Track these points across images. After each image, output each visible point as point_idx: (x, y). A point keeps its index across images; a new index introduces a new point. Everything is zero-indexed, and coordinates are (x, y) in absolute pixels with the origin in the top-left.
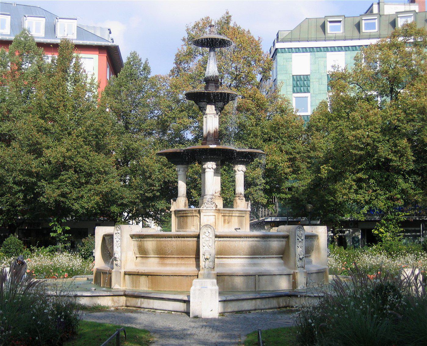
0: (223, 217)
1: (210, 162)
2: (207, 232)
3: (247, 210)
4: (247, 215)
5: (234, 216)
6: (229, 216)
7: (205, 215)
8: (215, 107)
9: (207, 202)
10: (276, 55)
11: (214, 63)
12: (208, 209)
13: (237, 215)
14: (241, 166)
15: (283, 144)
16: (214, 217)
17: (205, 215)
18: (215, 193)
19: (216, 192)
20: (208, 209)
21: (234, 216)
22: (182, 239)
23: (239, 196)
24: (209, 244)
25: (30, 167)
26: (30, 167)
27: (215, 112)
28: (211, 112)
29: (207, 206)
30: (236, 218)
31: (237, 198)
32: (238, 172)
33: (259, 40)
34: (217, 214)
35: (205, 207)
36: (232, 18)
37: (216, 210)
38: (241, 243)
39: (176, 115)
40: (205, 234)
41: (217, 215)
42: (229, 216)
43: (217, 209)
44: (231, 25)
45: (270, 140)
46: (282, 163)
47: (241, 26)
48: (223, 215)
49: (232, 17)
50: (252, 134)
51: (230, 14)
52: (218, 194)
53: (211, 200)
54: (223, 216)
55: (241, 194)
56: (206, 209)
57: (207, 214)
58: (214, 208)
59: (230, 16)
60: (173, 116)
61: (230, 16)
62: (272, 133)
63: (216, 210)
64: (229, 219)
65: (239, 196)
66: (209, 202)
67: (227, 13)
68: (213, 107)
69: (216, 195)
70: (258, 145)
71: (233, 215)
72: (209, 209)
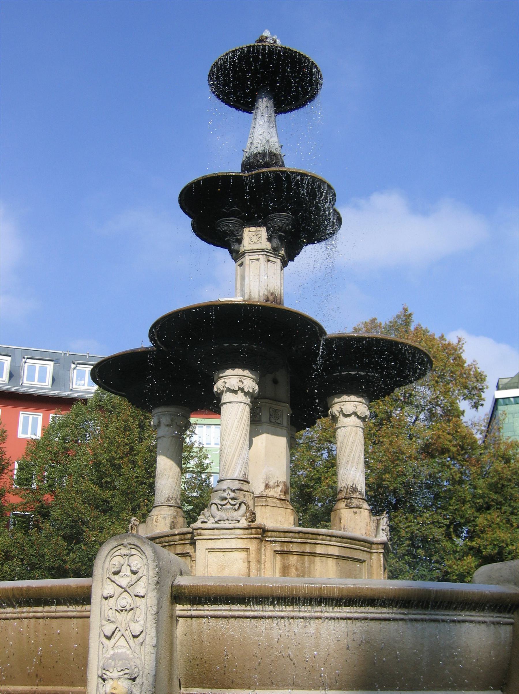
0: (278, 558)
1: (233, 367)
2: (126, 571)
3: (375, 540)
4: (374, 557)
5: (322, 555)
6: (302, 554)
7: (211, 550)
8: (268, 231)
9: (218, 502)
10: (497, 409)
11: (267, 124)
12: (222, 525)
13: (335, 551)
14: (353, 398)
15: (512, 513)
16: (243, 554)
17: (211, 550)
18: (267, 486)
19: (271, 484)
20: (222, 525)
21: (322, 555)
22: (40, 609)
23: (346, 498)
24: (132, 625)
25: (62, 560)
26: (62, 560)
27: (267, 245)
28: (255, 247)
29: (219, 514)
30: (331, 563)
31: (342, 505)
32: (342, 421)
33: (459, 342)
34: (255, 543)
35: (212, 520)
36: (414, 317)
37: (249, 528)
38: (297, 626)
39: (321, 475)
40: (116, 578)
41: (253, 546)
42: (302, 554)
43: (253, 525)
44: (412, 328)
45: (488, 508)
46: (513, 545)
47: (429, 329)
48: (278, 549)
49: (412, 316)
50: (454, 498)
51: (409, 312)
52: (277, 492)
53: (233, 495)
54: (281, 553)
55: (354, 490)
56: (216, 525)
57: (219, 544)
58: (244, 523)
59: (410, 315)
60: (318, 476)
61: (410, 315)
62: (491, 494)
63: (249, 528)
64: (303, 564)
65: (346, 498)
66: (225, 502)
67: (405, 310)
68: (263, 231)
69: (271, 493)
70: (467, 516)
71: (319, 550)
72: (227, 525)
